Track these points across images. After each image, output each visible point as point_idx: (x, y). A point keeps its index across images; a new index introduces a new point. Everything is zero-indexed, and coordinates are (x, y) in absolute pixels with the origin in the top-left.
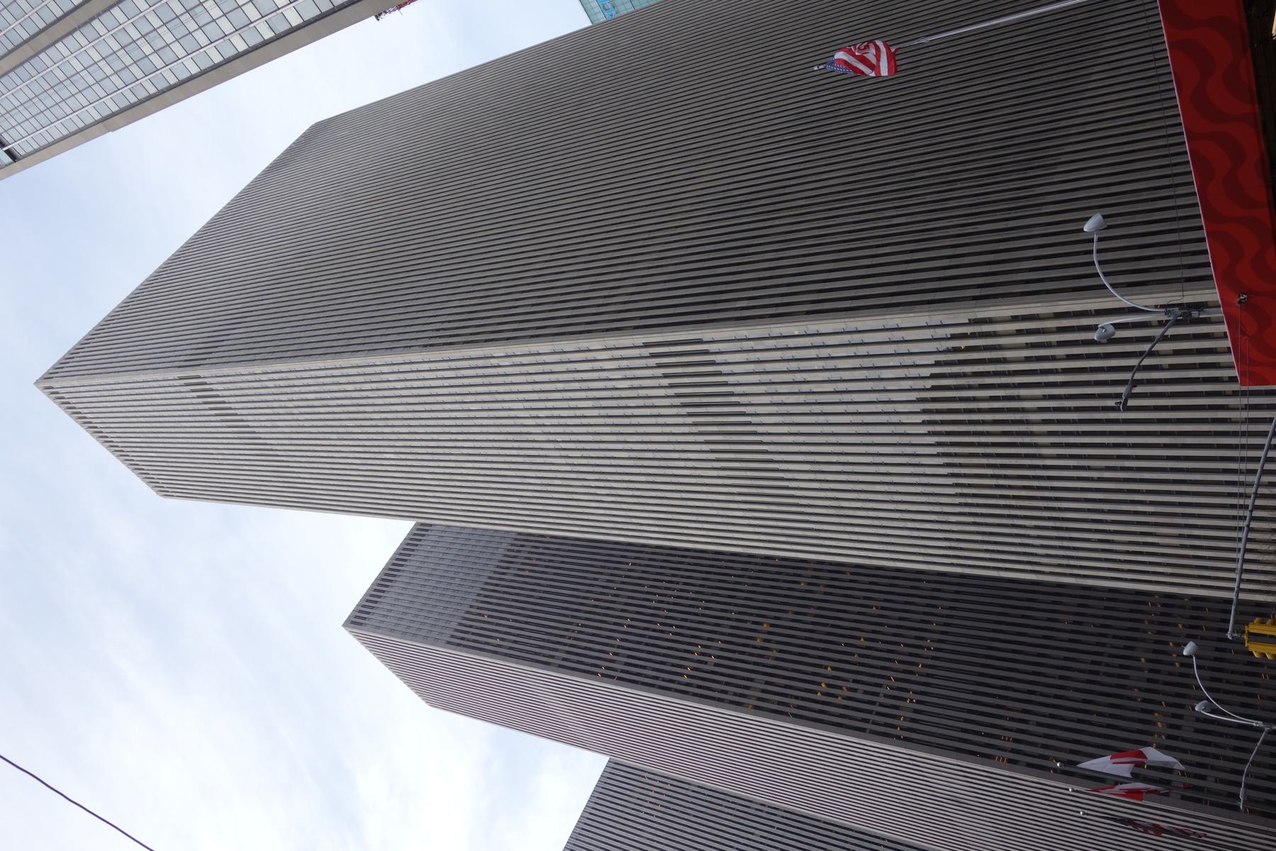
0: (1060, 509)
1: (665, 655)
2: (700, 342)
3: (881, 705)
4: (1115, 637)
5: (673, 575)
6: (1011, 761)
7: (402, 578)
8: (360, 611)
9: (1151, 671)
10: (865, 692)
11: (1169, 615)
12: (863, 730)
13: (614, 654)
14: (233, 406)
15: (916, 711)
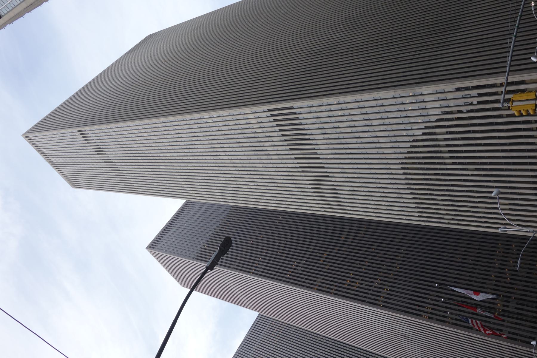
0: (453, 191)
1: (280, 266)
2: (292, 108)
3: (373, 291)
4: (481, 266)
5: (287, 232)
6: (429, 318)
7: (173, 229)
8: (154, 243)
9: (496, 281)
10: (366, 285)
11: (506, 257)
12: (364, 301)
13: (259, 264)
14: (118, 166)
15: (388, 294)
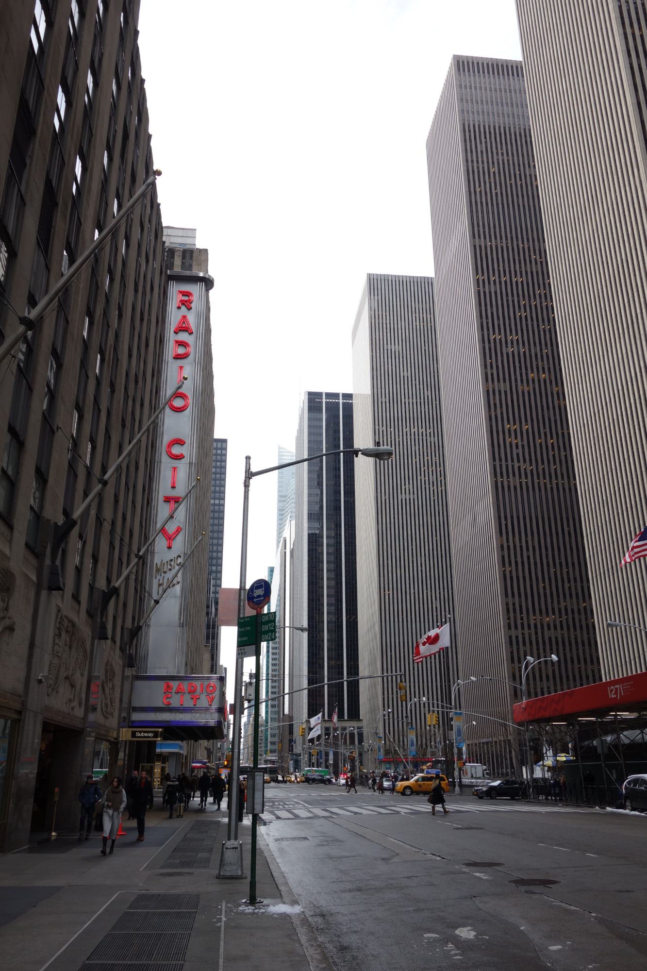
6: (502, 546)
12: (494, 460)
